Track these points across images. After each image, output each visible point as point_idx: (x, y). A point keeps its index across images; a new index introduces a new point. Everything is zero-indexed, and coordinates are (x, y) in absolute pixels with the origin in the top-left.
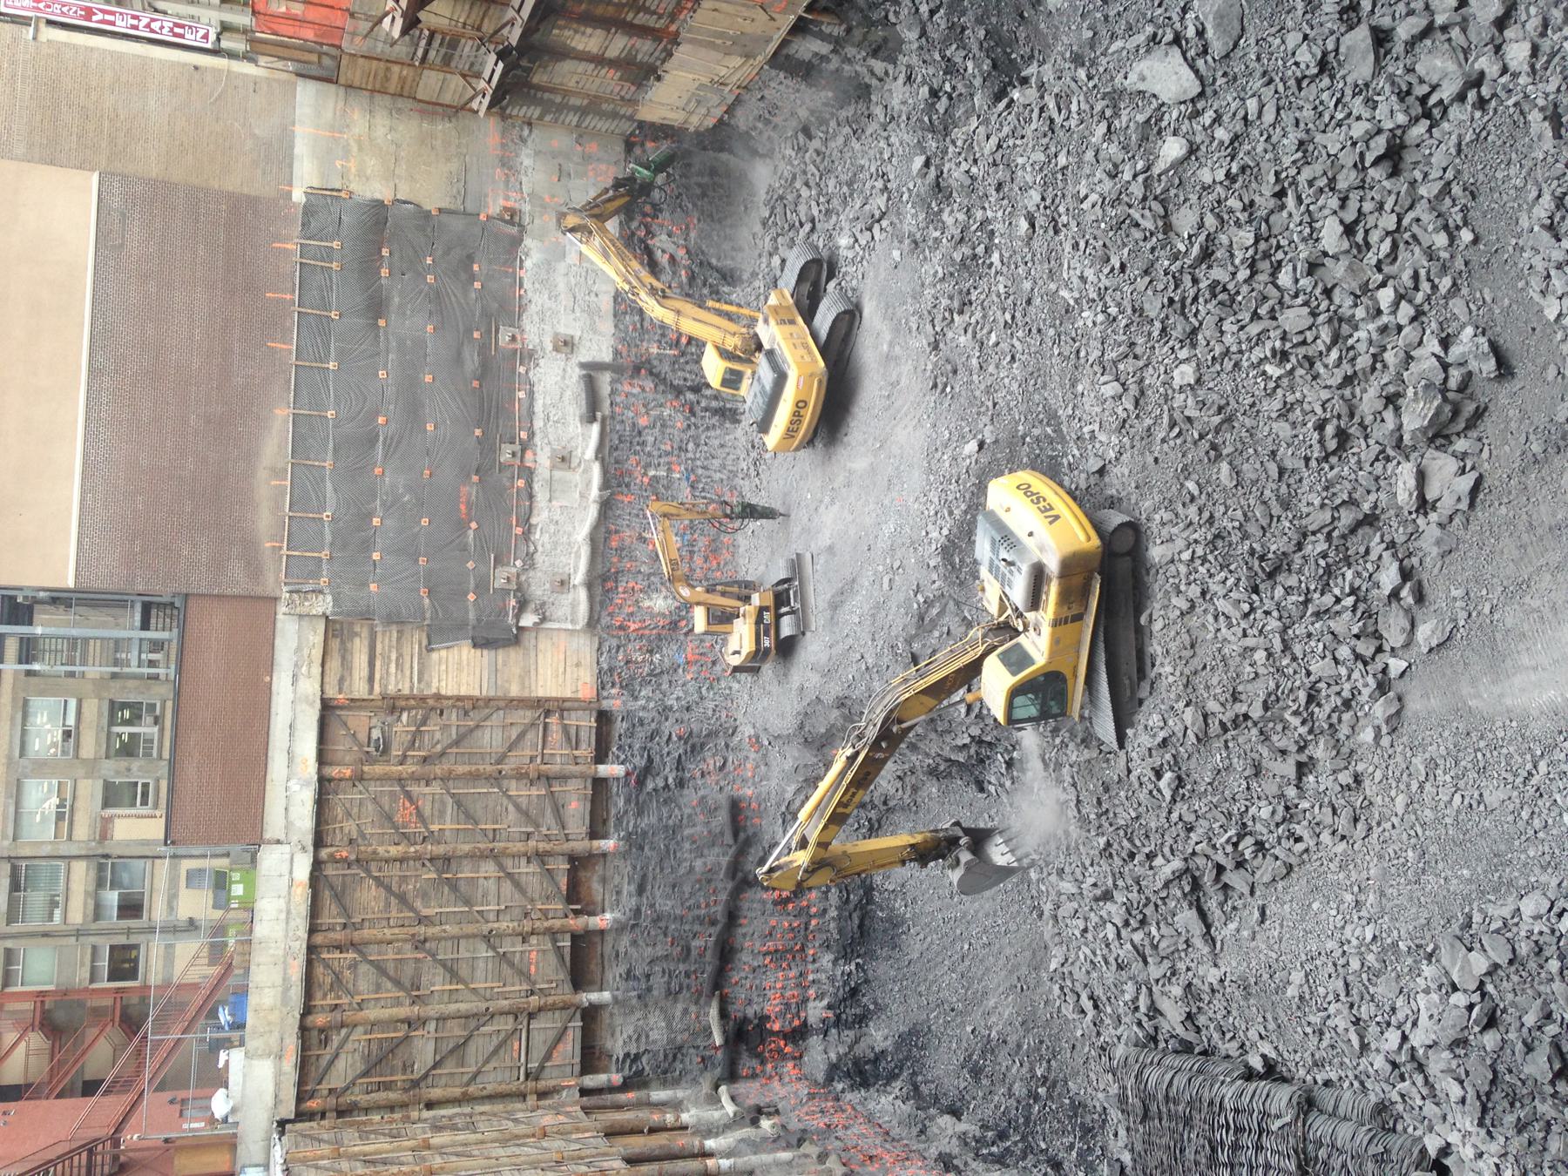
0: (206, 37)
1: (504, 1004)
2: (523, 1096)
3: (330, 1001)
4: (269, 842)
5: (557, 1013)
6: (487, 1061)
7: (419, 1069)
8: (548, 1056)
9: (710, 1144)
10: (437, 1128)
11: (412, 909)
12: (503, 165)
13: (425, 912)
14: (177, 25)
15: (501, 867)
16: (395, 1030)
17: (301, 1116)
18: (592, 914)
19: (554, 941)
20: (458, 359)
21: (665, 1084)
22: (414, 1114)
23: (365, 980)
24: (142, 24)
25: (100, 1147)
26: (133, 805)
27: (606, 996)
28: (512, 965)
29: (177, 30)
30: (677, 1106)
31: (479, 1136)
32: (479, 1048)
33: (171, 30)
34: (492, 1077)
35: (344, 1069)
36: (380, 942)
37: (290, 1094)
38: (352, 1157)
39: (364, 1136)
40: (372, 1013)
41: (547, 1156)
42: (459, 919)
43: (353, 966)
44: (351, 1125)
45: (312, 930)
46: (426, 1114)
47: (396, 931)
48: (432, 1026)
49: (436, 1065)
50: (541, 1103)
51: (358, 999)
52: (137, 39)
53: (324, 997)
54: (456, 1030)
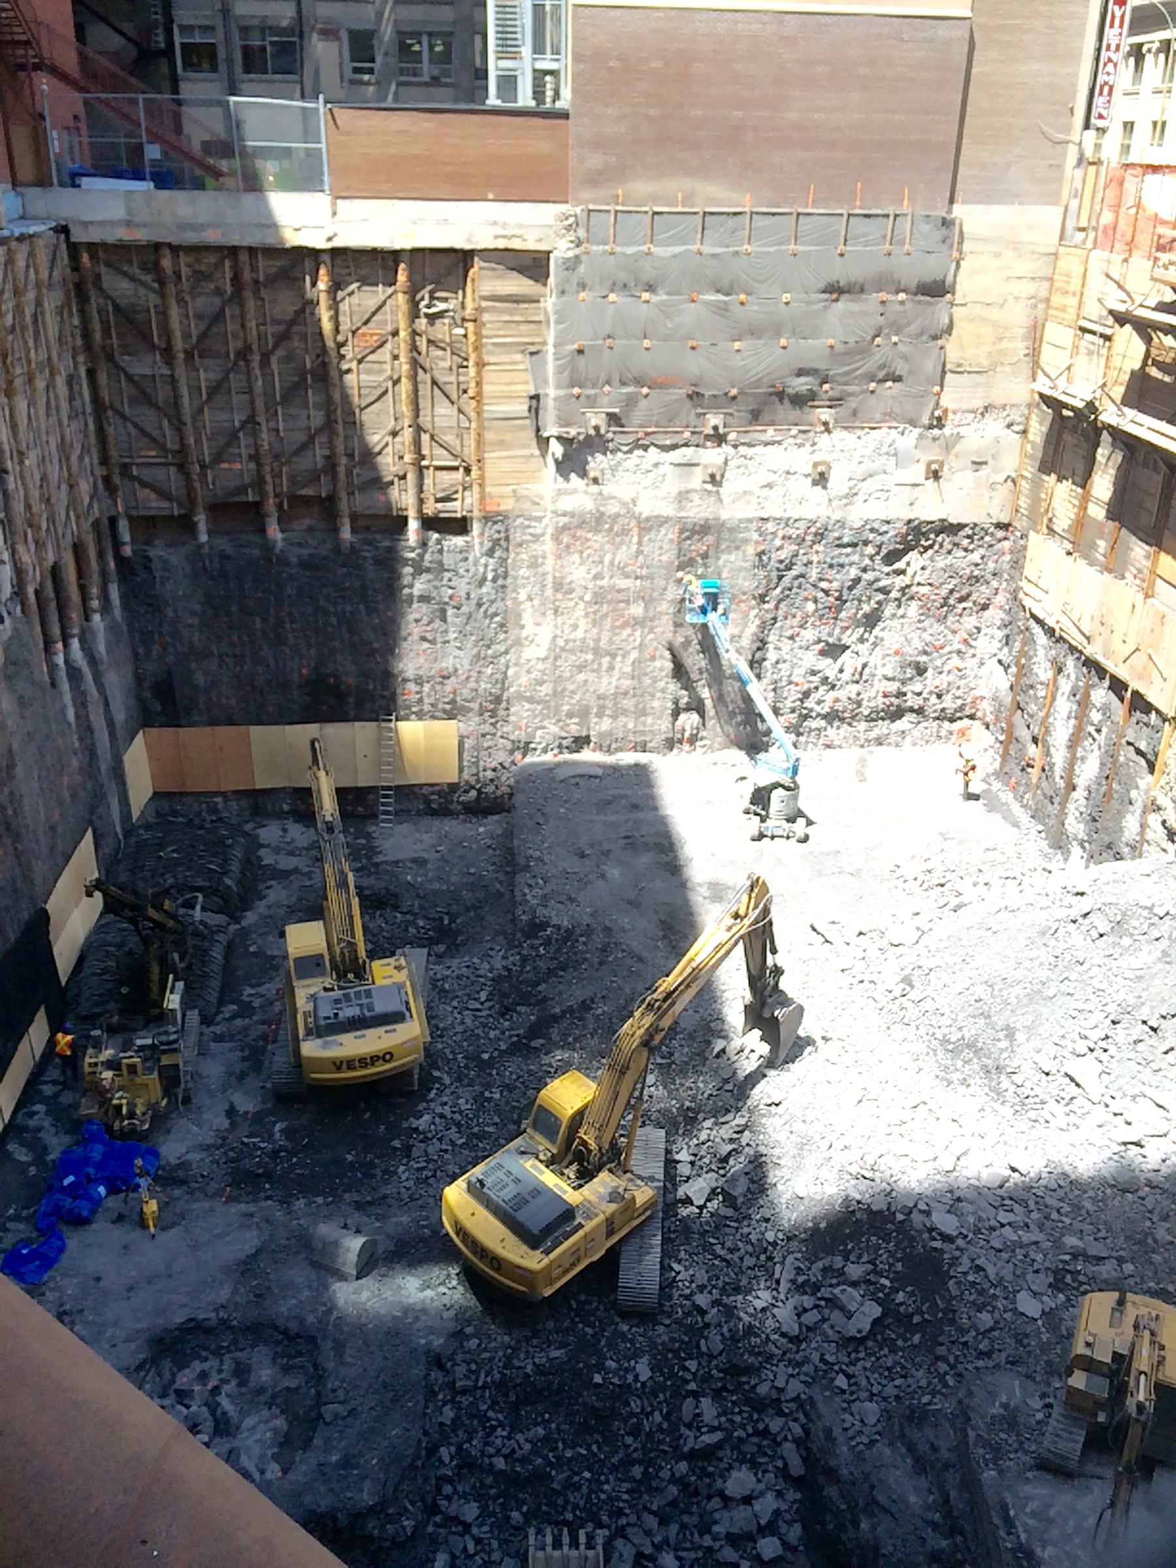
0: (1101, 117)
1: (191, 440)
2: (104, 461)
3: (185, 271)
4: (334, 205)
5: (184, 491)
6: (135, 425)
7: (125, 360)
8: (145, 484)
9: (75, 643)
10: (71, 381)
11: (275, 347)
12: (986, 408)
13: (274, 360)
14: (1111, 88)
15: (319, 431)
16: (160, 336)
17: (74, 249)
18: (279, 522)
19: (251, 485)
20: (801, 373)
21: (123, 597)
22: (81, 359)
23: (204, 303)
24: (1111, 54)
25: (31, 52)
26: (353, 60)
27: (204, 538)
28: (228, 445)
29: (1106, 89)
30: (106, 608)
31: (66, 423)
32: (148, 418)
33: (1106, 83)
34: (121, 430)
35: (120, 287)
36: (243, 317)
37: (95, 236)
38: (39, 303)
39: (60, 311)
40: (174, 313)
41: (52, 491)
42: (269, 392)
43: (218, 292)
44: (68, 297)
45: (252, 251)
46: (82, 371)
47: (254, 333)
48: (166, 371)
49: (130, 378)
50: (100, 481)
51: (188, 298)
52: (1099, 50)
53: (189, 266)
54: (162, 394)
